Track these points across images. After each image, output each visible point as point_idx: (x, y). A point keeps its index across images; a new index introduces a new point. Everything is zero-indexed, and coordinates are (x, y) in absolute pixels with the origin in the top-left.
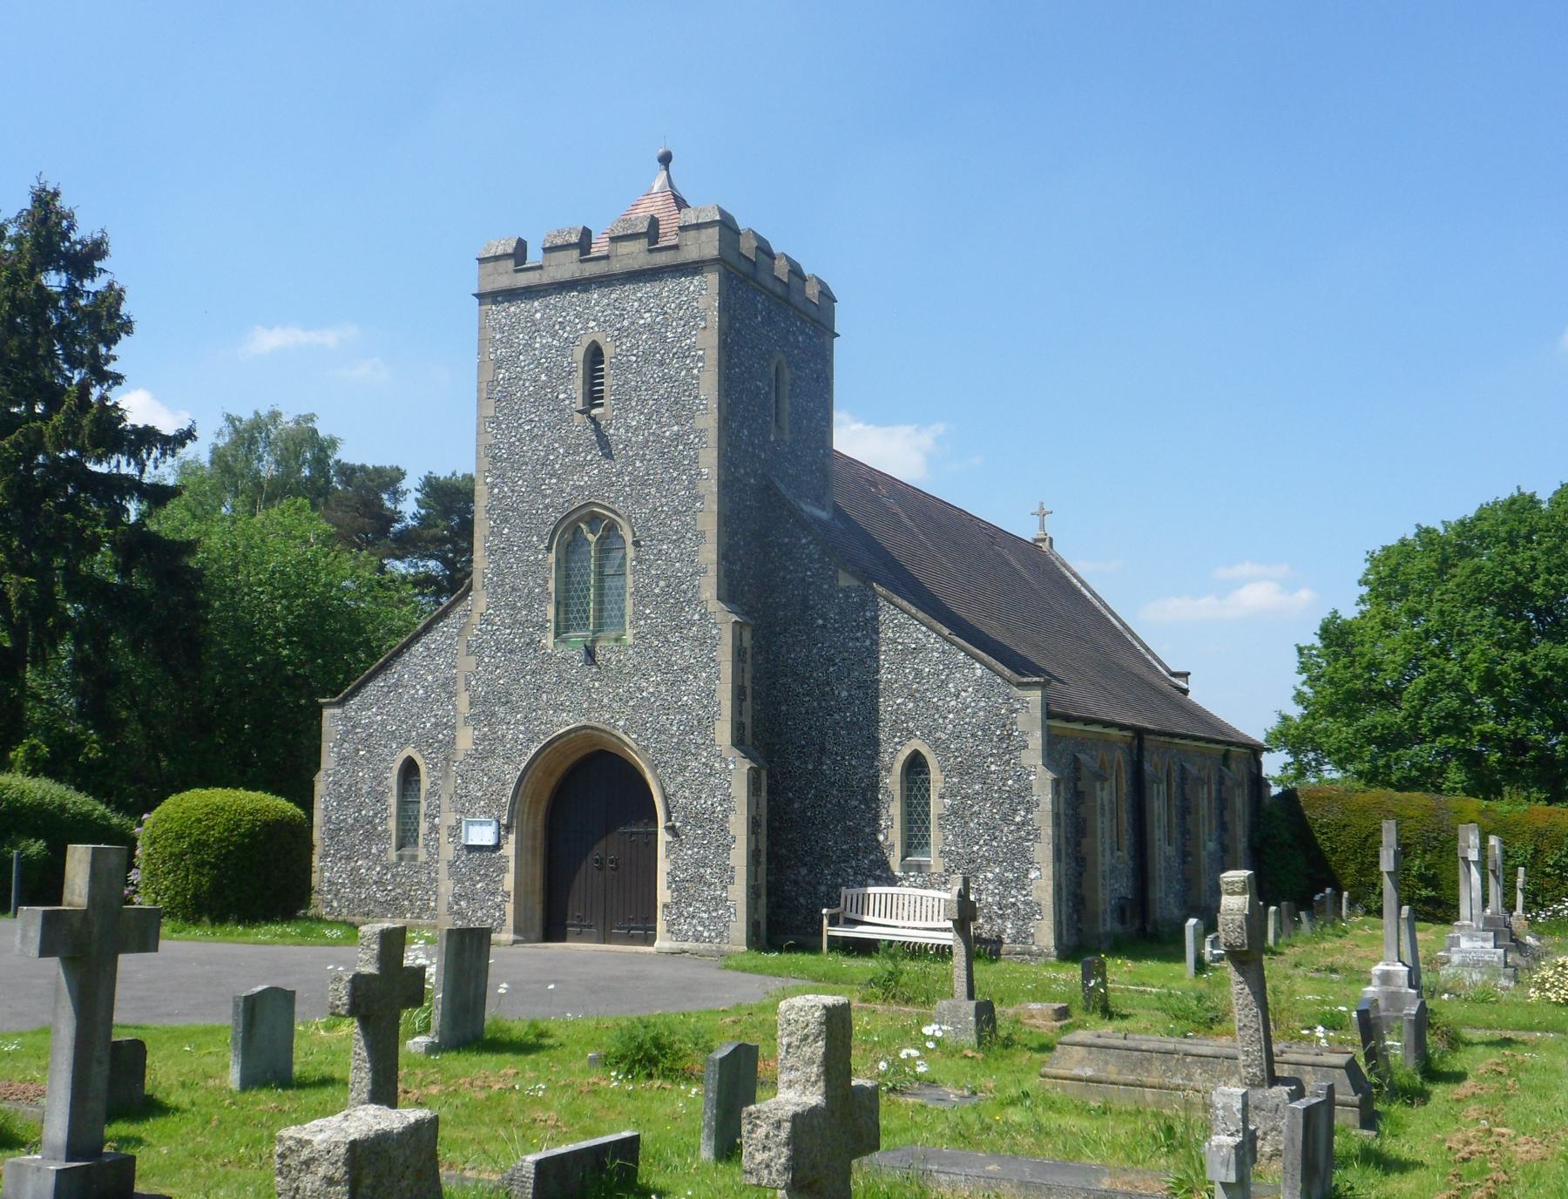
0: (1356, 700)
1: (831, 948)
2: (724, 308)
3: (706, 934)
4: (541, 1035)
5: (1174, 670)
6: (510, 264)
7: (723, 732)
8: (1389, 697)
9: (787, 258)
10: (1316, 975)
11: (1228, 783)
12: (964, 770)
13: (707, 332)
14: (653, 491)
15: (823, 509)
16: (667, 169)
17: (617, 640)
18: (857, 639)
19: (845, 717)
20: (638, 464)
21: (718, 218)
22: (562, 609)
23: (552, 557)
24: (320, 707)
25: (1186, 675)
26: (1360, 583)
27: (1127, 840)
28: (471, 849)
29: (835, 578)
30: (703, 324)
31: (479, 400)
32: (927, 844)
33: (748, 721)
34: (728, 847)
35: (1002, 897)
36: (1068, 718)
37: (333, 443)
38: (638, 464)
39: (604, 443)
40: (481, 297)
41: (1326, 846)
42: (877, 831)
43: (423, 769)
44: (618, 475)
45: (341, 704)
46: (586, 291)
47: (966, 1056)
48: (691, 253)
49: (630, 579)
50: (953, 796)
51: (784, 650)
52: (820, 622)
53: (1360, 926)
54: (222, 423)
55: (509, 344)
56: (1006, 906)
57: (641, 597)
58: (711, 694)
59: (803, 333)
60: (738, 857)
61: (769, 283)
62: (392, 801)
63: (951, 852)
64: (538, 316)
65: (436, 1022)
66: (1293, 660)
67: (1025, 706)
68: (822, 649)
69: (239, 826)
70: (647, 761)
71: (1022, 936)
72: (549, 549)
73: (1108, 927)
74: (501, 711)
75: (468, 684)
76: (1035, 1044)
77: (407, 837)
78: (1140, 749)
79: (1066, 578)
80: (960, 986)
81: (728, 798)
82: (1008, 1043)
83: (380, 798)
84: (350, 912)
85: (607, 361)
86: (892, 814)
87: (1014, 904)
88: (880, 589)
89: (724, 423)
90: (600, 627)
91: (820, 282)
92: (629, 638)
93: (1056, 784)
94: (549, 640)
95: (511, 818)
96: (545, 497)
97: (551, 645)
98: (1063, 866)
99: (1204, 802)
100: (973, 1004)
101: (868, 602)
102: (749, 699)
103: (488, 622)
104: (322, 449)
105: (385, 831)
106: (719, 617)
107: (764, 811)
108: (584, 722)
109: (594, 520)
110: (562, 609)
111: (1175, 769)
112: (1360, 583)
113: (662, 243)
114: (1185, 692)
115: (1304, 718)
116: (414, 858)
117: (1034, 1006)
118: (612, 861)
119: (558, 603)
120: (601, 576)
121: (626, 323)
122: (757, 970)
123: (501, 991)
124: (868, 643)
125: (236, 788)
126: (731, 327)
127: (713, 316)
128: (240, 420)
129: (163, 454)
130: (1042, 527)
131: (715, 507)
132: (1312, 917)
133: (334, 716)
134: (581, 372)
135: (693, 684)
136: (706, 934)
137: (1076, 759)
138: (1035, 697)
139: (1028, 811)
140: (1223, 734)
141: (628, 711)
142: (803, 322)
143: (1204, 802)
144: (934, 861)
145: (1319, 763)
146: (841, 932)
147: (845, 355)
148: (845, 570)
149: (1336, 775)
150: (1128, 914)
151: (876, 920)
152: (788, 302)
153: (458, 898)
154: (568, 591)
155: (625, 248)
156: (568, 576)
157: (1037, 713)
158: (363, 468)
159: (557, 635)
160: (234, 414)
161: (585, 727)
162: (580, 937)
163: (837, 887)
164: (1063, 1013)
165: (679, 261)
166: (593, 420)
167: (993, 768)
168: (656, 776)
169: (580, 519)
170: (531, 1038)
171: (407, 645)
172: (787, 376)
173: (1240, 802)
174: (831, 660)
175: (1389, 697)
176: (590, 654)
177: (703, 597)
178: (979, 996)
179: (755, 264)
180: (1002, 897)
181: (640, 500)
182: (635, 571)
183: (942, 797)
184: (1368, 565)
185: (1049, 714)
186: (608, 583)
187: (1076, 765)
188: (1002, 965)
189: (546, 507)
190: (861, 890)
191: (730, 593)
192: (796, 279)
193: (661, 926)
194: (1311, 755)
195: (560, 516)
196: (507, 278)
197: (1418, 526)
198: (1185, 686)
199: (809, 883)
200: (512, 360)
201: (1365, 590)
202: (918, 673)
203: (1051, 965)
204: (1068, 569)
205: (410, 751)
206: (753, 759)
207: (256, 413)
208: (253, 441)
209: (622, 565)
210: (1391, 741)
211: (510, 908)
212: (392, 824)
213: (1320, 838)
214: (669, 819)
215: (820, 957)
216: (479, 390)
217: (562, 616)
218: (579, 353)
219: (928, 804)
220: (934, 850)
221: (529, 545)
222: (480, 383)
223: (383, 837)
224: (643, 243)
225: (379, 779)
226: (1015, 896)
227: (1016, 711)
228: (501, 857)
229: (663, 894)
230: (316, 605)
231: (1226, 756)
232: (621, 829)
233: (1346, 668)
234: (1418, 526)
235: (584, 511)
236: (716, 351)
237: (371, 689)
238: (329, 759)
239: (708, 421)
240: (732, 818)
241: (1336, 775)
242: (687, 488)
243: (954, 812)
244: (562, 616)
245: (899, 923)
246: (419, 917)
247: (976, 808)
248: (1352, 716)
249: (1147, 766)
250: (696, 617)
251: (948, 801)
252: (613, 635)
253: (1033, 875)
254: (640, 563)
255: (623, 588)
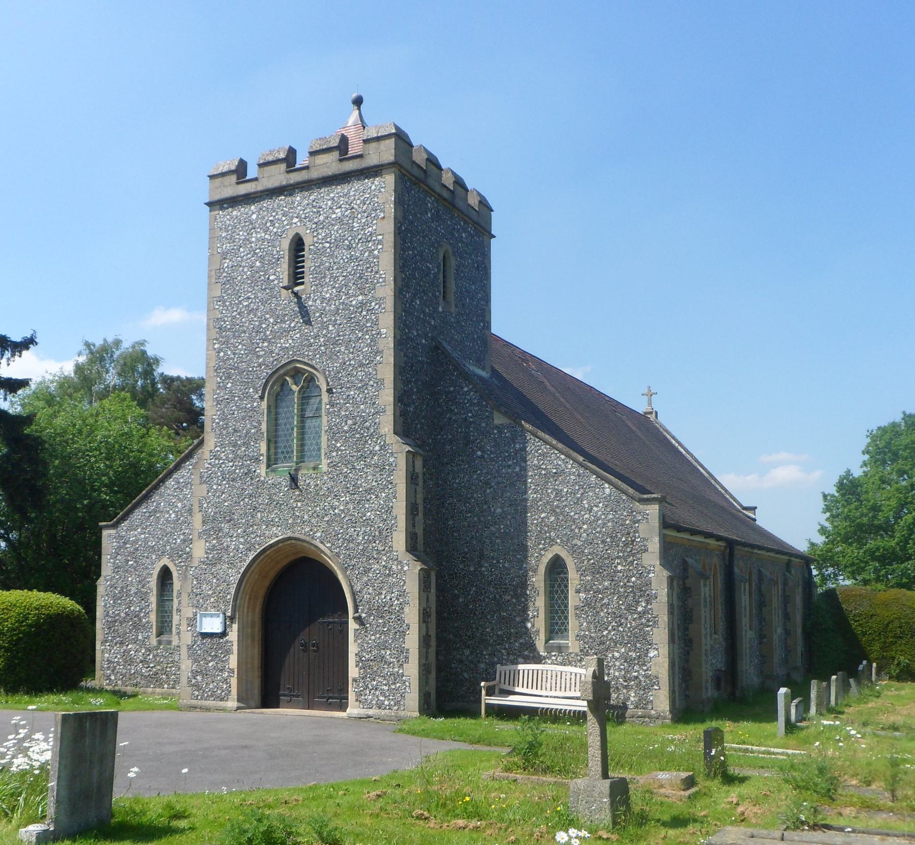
0: (862, 531)
1: (488, 714)
2: (399, 202)
3: (386, 703)
4: (178, 816)
5: (745, 505)
6: (233, 178)
7: (399, 540)
8: (887, 529)
9: (453, 173)
10: (883, 733)
11: (791, 583)
12: (596, 571)
13: (385, 221)
14: (343, 349)
15: (483, 369)
16: (359, 109)
17: (315, 468)
18: (509, 466)
19: (499, 529)
20: (331, 328)
21: (394, 131)
22: (272, 446)
23: (264, 404)
24: (100, 529)
25: (753, 509)
26: (863, 453)
27: (721, 626)
28: (205, 635)
29: (490, 418)
30: (382, 215)
31: (209, 284)
32: (566, 630)
33: (419, 530)
34: (403, 634)
35: (627, 672)
36: (679, 529)
37: (157, 361)
38: (331, 328)
39: (304, 313)
40: (211, 204)
41: (859, 630)
42: (526, 619)
43: (175, 575)
44: (316, 337)
45: (115, 526)
46: (291, 195)
47: (600, 838)
48: (373, 159)
49: (325, 419)
50: (587, 591)
51: (451, 477)
52: (479, 453)
53: (888, 687)
54: (82, 347)
55: (232, 240)
56: (630, 679)
57: (334, 433)
58: (389, 510)
59: (465, 230)
60: (412, 641)
61: (438, 189)
62: (153, 599)
63: (585, 636)
64: (254, 216)
65: (51, 811)
66: (821, 505)
67: (645, 516)
68: (480, 475)
69: (27, 619)
70: (338, 564)
71: (643, 703)
72: (262, 398)
73: (709, 694)
74: (226, 527)
75: (201, 506)
76: (666, 818)
77: (164, 627)
78: (731, 555)
79: (666, 438)
80: (595, 764)
81: (403, 594)
82: (643, 819)
83: (144, 597)
84: (123, 683)
85: (306, 248)
86: (538, 605)
87: (636, 677)
88: (527, 426)
89: (399, 293)
90: (301, 458)
91: (479, 194)
92: (324, 467)
93: (671, 580)
94: (262, 470)
95: (234, 610)
96: (259, 357)
97: (263, 474)
98: (676, 646)
99: (775, 601)
100: (607, 783)
101: (518, 436)
102: (421, 515)
103: (217, 458)
104: (149, 365)
105: (148, 622)
106: (395, 448)
107: (433, 605)
108: (289, 534)
109: (296, 373)
110: (272, 446)
111: (755, 571)
112: (863, 453)
113: (351, 152)
114: (755, 520)
115: (826, 544)
116: (169, 643)
117: (663, 776)
118: (314, 645)
119: (269, 441)
120: (302, 418)
121: (321, 218)
122: (425, 734)
123: (131, 775)
124: (517, 469)
125: (31, 589)
126: (405, 218)
127: (390, 208)
128: (94, 346)
129: (13, 355)
130: (650, 404)
131: (392, 360)
132: (859, 683)
133: (110, 535)
134: (287, 258)
135: (375, 503)
136: (386, 703)
137: (685, 562)
138: (653, 510)
139: (648, 602)
140: (786, 548)
141: (324, 525)
142: (465, 222)
143: (775, 601)
144: (572, 643)
145: (836, 575)
146: (495, 700)
147: (497, 249)
148: (499, 411)
149: (848, 582)
150: (723, 683)
151: (534, 692)
152: (454, 206)
153: (195, 674)
154: (276, 431)
155: (322, 159)
156: (276, 419)
157: (655, 523)
158: (178, 378)
159: (268, 466)
160: (90, 341)
161: (290, 538)
162: (290, 704)
163: (493, 665)
164: (689, 782)
165: (364, 166)
166: (296, 294)
167: (620, 568)
168: (346, 577)
169: (286, 374)
170: (163, 822)
171: (163, 481)
172: (453, 262)
173: (798, 599)
174: (487, 483)
175: (887, 529)
176: (294, 480)
177: (383, 432)
178: (614, 774)
179: (425, 172)
180: (627, 672)
181: (332, 356)
182: (328, 413)
183: (578, 591)
184: (869, 440)
185: (665, 524)
186: (308, 423)
187: (685, 567)
188: (624, 727)
189: (260, 365)
190: (512, 667)
191: (404, 429)
192: (459, 190)
193: (352, 696)
194: (831, 570)
195: (270, 372)
196: (231, 188)
197: (904, 413)
198: (753, 516)
199: (471, 662)
200: (235, 252)
201: (867, 457)
202: (558, 493)
203: (668, 727)
204: (669, 433)
205: (165, 561)
206: (424, 562)
207: (105, 340)
208: (102, 359)
209: (319, 409)
210: (886, 558)
211: (234, 681)
212: (153, 617)
213: (854, 625)
214: (356, 611)
215: (479, 721)
216: (209, 277)
217: (272, 451)
218: (286, 244)
219: (566, 598)
220: (571, 634)
221: (247, 396)
222: (210, 271)
223: (146, 627)
224: (335, 155)
225: (143, 582)
226: (637, 671)
227: (638, 521)
228: (227, 642)
229: (353, 671)
230: (132, 465)
231: (788, 565)
232: (321, 620)
233: (857, 509)
234: (904, 413)
235: (289, 367)
236: (392, 236)
237: (137, 514)
238: (107, 569)
239: (386, 291)
240: (407, 609)
241: (848, 582)
242: (369, 345)
243: (587, 603)
244: (272, 451)
245: (544, 693)
246: (173, 688)
247: (606, 601)
248: (861, 543)
249: (736, 570)
250: (377, 448)
251: (582, 595)
252: (312, 465)
253: (652, 654)
254: (332, 406)
255: (320, 426)
